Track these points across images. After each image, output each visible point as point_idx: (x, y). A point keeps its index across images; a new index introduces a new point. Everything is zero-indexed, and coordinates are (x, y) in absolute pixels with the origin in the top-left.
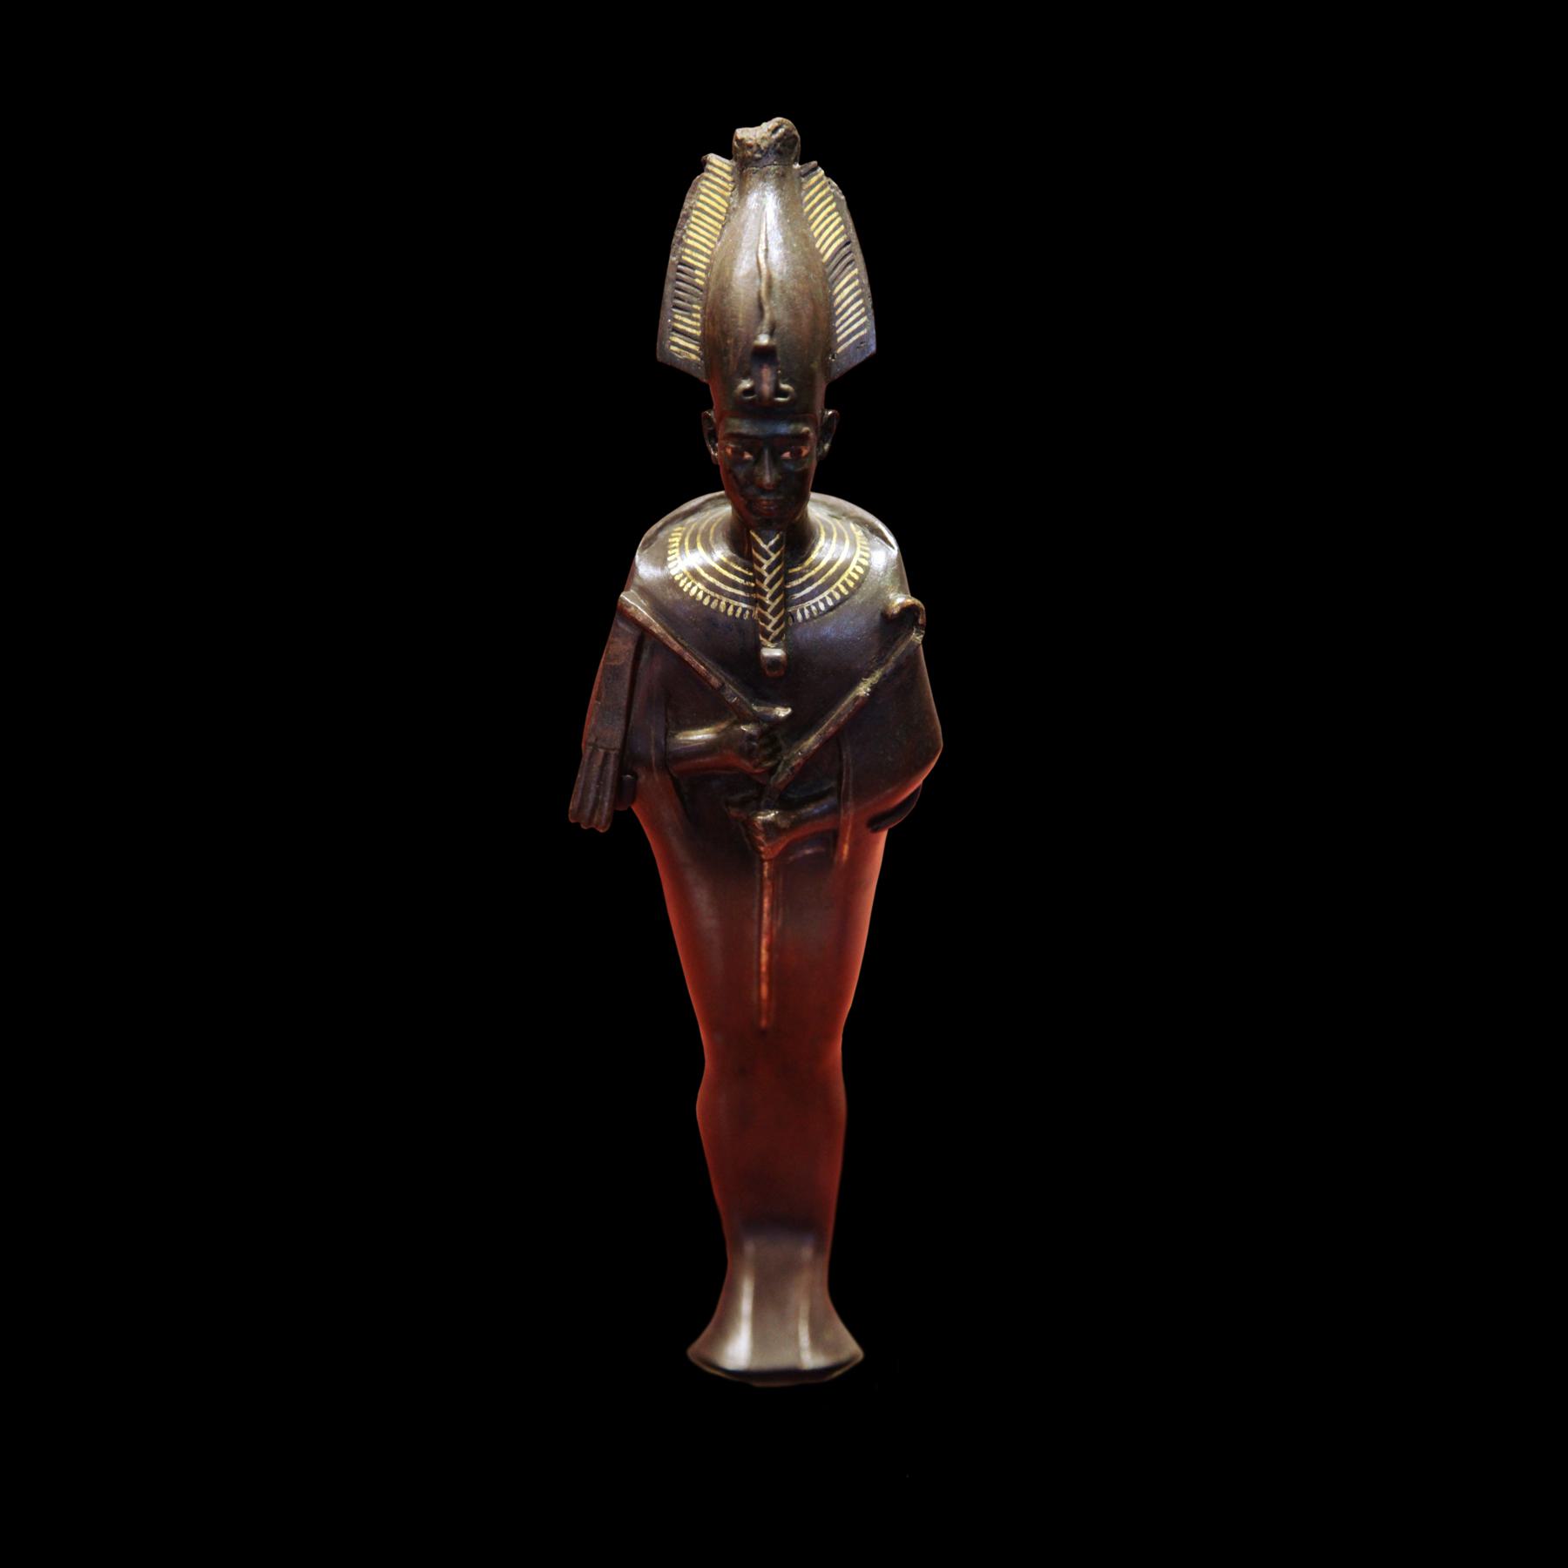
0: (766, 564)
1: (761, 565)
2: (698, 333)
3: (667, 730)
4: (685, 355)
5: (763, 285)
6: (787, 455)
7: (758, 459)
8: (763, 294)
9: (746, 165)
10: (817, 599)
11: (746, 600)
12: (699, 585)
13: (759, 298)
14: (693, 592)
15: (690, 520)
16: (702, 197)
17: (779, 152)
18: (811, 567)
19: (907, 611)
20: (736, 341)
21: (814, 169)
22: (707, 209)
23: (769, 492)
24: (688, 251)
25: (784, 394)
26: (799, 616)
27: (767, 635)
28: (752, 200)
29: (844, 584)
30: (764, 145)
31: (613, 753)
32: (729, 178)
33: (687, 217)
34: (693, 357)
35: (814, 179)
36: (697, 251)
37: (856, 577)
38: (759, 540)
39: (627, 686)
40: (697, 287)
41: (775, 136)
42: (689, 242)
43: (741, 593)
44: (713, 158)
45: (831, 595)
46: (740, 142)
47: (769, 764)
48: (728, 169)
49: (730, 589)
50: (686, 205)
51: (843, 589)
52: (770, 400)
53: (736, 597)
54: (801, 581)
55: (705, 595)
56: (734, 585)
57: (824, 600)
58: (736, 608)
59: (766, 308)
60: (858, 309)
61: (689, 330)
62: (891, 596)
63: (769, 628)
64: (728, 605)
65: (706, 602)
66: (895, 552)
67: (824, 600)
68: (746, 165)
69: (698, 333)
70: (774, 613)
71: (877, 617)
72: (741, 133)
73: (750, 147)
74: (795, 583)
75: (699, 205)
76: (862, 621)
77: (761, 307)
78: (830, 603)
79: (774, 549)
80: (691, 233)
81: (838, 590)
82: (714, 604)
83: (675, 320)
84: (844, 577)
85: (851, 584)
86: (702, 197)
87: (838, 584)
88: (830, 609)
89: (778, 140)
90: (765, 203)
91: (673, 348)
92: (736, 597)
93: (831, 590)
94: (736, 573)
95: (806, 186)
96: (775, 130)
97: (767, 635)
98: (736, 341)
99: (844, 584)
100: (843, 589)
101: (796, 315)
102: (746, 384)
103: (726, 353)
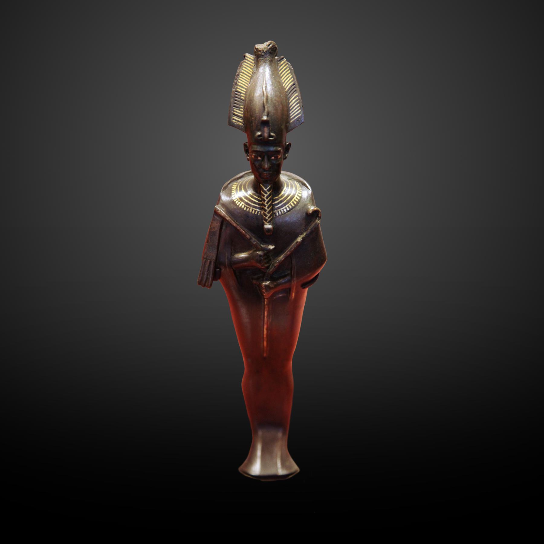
0: (266, 196)
1: (264, 196)
2: (242, 116)
3: (231, 253)
4: (238, 123)
5: (265, 99)
6: (273, 158)
7: (263, 159)
8: (265, 102)
9: (259, 57)
10: (283, 208)
11: (259, 208)
12: (243, 203)
13: (263, 103)
14: (240, 205)
15: (240, 180)
16: (244, 68)
17: (270, 53)
18: (281, 197)
19: (316, 213)
20: (255, 118)
21: (283, 59)
22: (245, 72)
23: (267, 171)
24: (239, 87)
25: (272, 137)
26: (277, 214)
27: (266, 220)
28: (261, 69)
29: (293, 202)
30: (265, 50)
31: (213, 261)
32: (253, 62)
33: (238, 75)
34: (241, 124)
35: (282, 62)
36: (242, 87)
37: (297, 200)
38: (263, 187)
39: (217, 238)
40: (242, 99)
41: (269, 47)
42: (239, 84)
43: (257, 206)
44: (247, 55)
45: (288, 207)
46: (257, 49)
47: (267, 265)
48: (253, 58)
49: (253, 204)
50: (238, 71)
51: (292, 204)
52: (267, 139)
53: (255, 207)
54: (278, 201)
55: (245, 206)
56: (255, 203)
57: (286, 208)
58: (255, 211)
59: (266, 107)
60: (298, 107)
61: (239, 114)
62: (309, 207)
63: (267, 218)
64: (253, 210)
65: (245, 209)
66: (310, 192)
67: (286, 208)
68: (259, 57)
69: (242, 116)
70: (269, 213)
71: (304, 214)
72: (257, 46)
73: (260, 51)
74: (276, 202)
75: (243, 71)
76: (299, 215)
77: (264, 107)
78: (288, 209)
79: (269, 190)
80: (240, 81)
81: (291, 205)
82: (248, 210)
83: (234, 111)
84: (293, 200)
85: (295, 203)
86: (244, 68)
87: (291, 203)
88: (288, 211)
89: (270, 49)
90: (265, 71)
91: (234, 121)
92: (255, 207)
93: (288, 205)
94: (255, 199)
95: (280, 65)
96: (269, 45)
97: (266, 220)
98: (255, 118)
99: (293, 202)
100: (292, 204)
101: (276, 109)
102: (259, 133)
103: (252, 122)
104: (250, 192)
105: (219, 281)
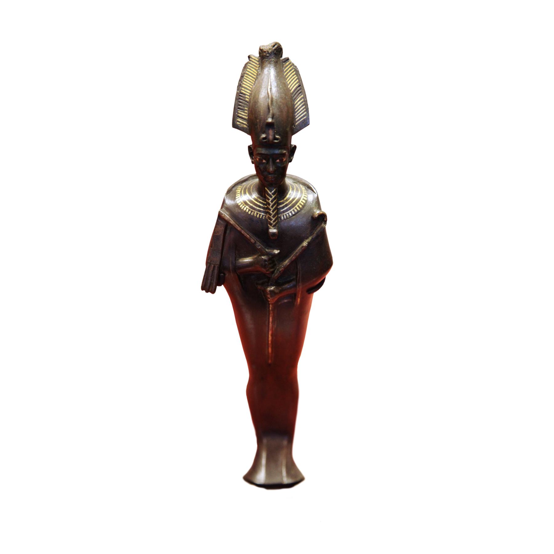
0: (271, 199)
1: (269, 199)
2: (247, 118)
5: (270, 101)
6: (278, 161)
7: (268, 162)
8: (270, 104)
9: (264, 58)
10: (289, 212)
11: (264, 212)
12: (247, 207)
13: (268, 105)
14: (245, 209)
15: (244, 184)
16: (248, 70)
17: (275, 54)
18: (287, 200)
20: (260, 121)
22: (250, 74)
23: (272, 174)
24: (243, 89)
25: (277, 139)
26: (282, 218)
27: (271, 224)
28: (266, 71)
29: (298, 206)
30: (270, 51)
31: (216, 266)
32: (258, 63)
34: (245, 126)
36: (246, 89)
37: (303, 204)
38: (268, 191)
39: (221, 242)
40: (246, 101)
41: (274, 48)
42: (244, 85)
43: (262, 210)
45: (293, 210)
47: (272, 270)
49: (258, 208)
51: (298, 208)
52: (272, 141)
53: (260, 211)
54: (283, 205)
55: (249, 210)
56: (259, 207)
57: (291, 212)
58: (260, 215)
59: (271, 109)
60: (303, 109)
61: (244, 117)
62: (315, 210)
63: (272, 222)
64: (257, 214)
65: (249, 213)
67: (291, 212)
69: (247, 118)
70: (273, 217)
71: (310, 218)
73: (265, 52)
74: (281, 206)
75: (247, 72)
76: (304, 219)
77: (269, 109)
78: (293, 213)
79: (273, 194)
80: (244, 82)
81: (296, 208)
82: (252, 213)
83: (239, 113)
84: (298, 204)
85: (301, 206)
86: (248, 70)
87: (296, 206)
88: (293, 215)
89: (275, 49)
91: (238, 123)
92: (260, 211)
93: (294, 208)
94: (260, 202)
95: (285, 66)
97: (271, 224)
98: (260, 121)
99: (298, 206)
100: (298, 208)
101: (281, 111)
102: (264, 136)
103: (256, 125)
104: (255, 195)
105: (223, 286)
